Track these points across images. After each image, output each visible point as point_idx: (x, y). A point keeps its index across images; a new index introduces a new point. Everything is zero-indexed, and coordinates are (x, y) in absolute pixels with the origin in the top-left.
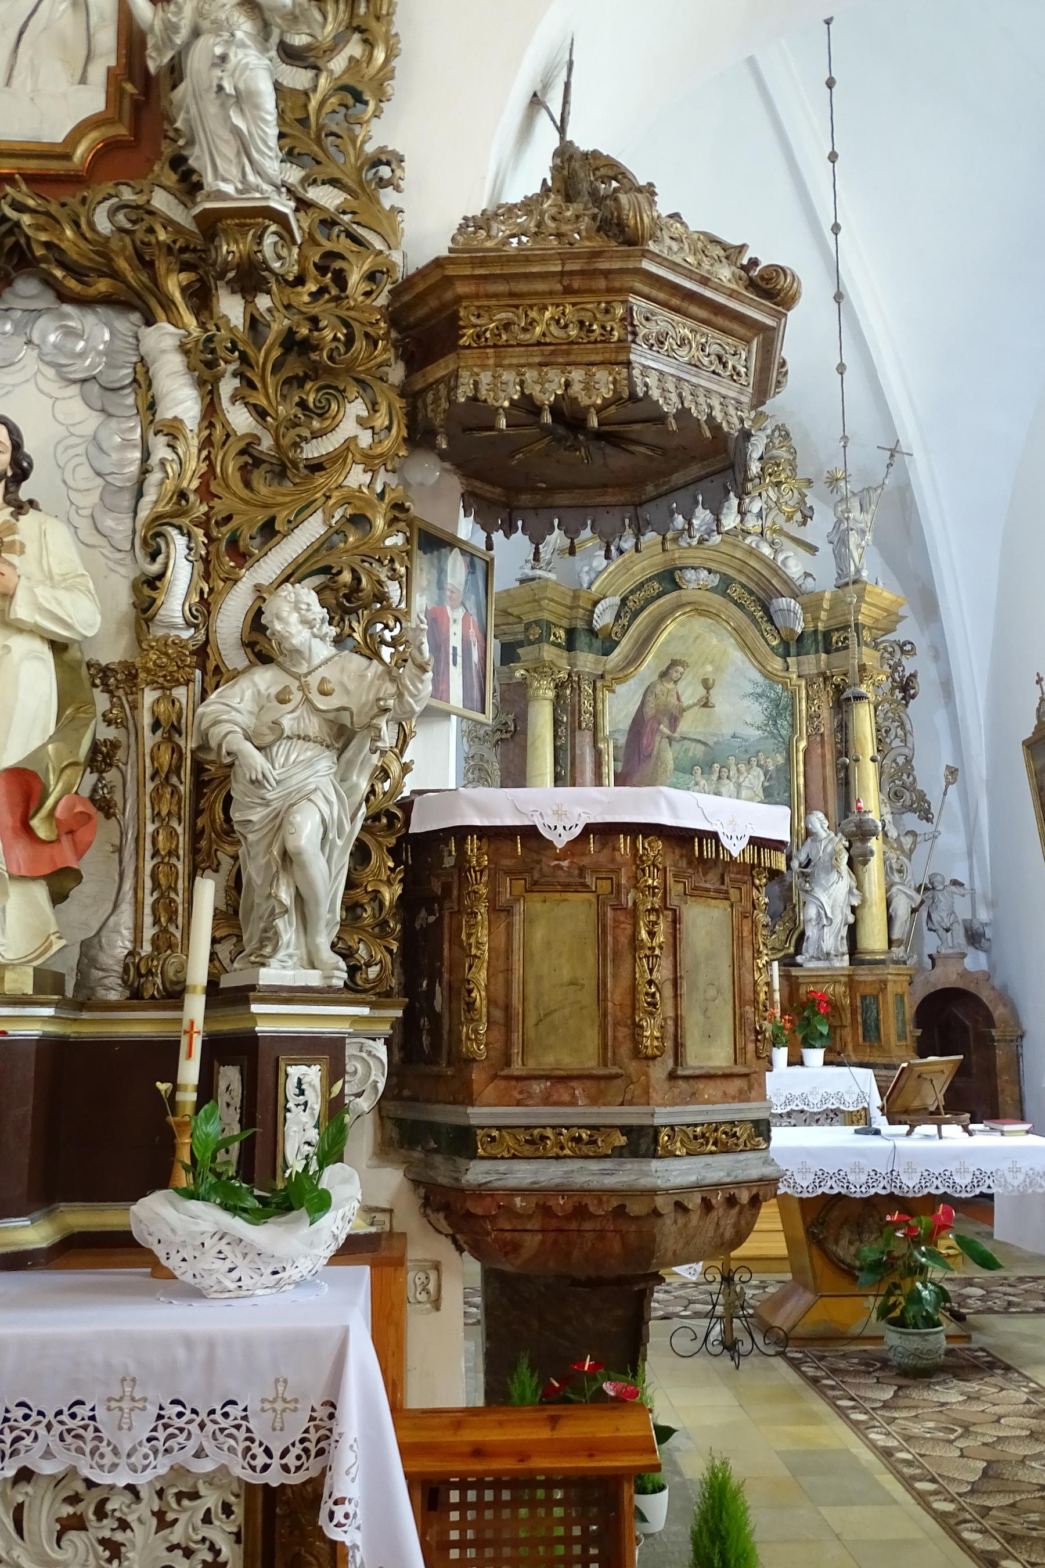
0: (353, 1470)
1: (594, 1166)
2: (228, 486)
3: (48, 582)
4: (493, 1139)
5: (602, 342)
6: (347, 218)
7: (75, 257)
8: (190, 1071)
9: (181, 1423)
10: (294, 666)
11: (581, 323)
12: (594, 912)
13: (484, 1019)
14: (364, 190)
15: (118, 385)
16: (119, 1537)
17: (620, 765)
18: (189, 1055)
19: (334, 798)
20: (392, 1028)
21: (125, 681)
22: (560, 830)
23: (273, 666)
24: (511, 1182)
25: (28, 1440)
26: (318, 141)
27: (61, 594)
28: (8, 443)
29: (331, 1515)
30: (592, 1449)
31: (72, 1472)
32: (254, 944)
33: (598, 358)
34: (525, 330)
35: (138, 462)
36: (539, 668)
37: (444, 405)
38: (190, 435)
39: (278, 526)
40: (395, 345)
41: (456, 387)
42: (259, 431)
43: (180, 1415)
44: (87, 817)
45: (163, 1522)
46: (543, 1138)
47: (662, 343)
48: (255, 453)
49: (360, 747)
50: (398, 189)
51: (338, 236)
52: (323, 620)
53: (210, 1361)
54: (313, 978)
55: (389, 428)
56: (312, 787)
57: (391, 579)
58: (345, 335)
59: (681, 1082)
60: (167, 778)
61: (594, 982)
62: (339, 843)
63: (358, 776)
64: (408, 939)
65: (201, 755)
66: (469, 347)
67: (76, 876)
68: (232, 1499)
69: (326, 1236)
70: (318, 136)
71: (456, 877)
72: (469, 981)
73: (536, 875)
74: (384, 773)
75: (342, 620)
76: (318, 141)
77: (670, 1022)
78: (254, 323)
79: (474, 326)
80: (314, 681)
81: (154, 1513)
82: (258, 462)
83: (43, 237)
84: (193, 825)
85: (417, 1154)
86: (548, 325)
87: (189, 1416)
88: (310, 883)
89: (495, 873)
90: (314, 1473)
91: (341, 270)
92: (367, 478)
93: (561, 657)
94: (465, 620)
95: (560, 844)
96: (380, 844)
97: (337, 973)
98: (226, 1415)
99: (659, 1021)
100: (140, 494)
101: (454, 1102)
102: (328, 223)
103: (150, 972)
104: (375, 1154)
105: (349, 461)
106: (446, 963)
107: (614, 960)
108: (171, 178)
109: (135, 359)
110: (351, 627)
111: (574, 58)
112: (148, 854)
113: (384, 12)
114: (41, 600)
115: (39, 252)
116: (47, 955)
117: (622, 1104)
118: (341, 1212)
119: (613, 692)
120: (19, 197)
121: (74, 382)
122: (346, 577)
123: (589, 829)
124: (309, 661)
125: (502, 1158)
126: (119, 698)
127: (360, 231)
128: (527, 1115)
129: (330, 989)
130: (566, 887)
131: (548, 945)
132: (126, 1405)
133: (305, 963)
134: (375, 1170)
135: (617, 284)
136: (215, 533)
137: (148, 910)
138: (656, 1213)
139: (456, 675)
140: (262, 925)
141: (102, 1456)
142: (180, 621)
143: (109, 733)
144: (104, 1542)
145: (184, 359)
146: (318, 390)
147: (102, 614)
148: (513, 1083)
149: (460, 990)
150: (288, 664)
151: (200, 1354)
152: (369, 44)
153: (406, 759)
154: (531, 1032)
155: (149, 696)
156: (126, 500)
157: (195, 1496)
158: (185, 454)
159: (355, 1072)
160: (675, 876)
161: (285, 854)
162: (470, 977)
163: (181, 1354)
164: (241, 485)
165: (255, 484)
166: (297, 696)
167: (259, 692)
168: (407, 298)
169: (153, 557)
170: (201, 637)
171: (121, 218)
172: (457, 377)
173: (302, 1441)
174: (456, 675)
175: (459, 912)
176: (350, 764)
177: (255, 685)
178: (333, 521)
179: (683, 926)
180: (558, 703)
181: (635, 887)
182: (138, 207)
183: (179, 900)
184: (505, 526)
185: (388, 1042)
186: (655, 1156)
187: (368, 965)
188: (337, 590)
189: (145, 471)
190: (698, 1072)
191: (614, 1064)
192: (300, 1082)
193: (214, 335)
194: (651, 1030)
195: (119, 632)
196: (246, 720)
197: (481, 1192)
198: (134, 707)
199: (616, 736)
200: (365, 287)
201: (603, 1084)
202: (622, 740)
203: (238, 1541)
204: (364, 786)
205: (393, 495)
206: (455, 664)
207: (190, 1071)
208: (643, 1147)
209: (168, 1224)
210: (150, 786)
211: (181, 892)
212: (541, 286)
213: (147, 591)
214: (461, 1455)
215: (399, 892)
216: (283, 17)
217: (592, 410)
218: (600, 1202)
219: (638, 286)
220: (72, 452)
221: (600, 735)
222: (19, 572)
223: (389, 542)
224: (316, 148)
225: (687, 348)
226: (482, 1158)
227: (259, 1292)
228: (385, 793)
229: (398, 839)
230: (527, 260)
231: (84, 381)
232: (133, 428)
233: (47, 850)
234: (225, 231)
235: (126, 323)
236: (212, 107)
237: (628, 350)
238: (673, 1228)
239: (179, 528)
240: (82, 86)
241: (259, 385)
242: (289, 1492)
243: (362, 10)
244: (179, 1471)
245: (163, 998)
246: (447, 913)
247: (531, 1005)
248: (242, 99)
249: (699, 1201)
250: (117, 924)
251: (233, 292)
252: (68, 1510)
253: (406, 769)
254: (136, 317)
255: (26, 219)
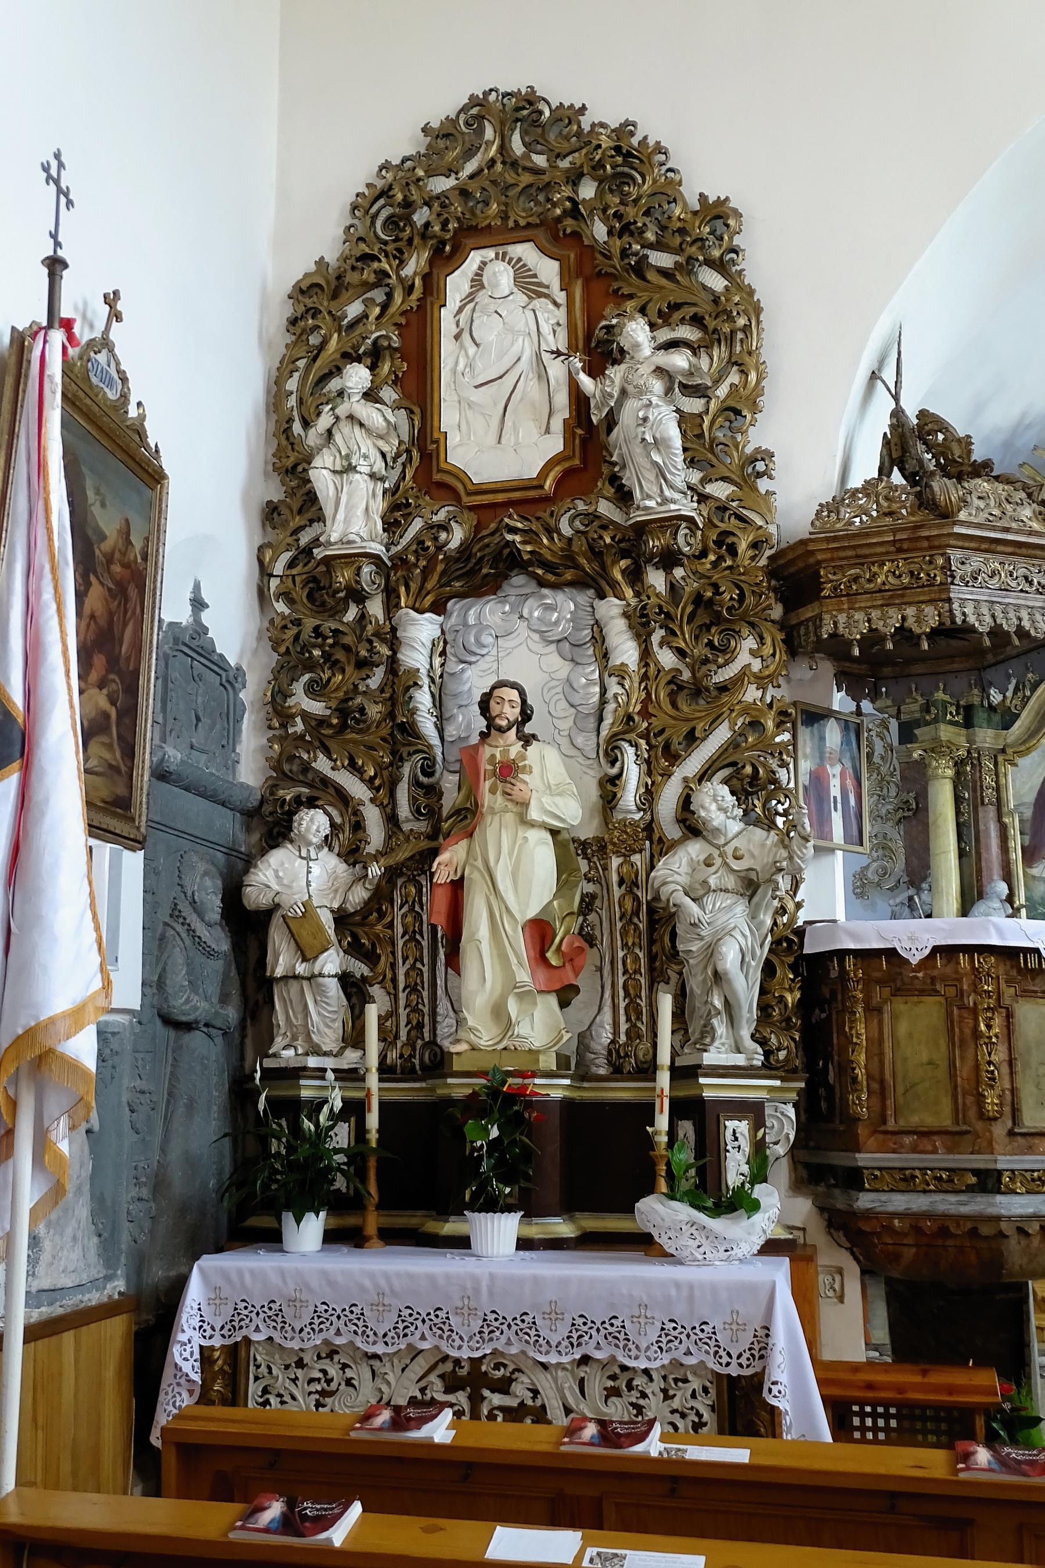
0: (782, 1366)
1: (952, 1198)
2: (661, 708)
3: (548, 791)
4: (876, 1177)
5: (928, 586)
6: (734, 504)
7: (549, 558)
8: (662, 1122)
9: (675, 1333)
10: (715, 838)
11: (912, 573)
12: (943, 1010)
13: (865, 1090)
14: (746, 482)
15: (581, 642)
16: (641, 1402)
17: (1027, 838)
18: (662, 1111)
19: (748, 933)
20: (798, 1095)
21: (598, 851)
22: (914, 951)
23: (700, 838)
24: (890, 1208)
25: (586, 1338)
26: (712, 451)
27: (558, 800)
28: (519, 701)
29: (770, 1391)
30: (951, 1390)
31: (613, 1359)
32: (697, 1035)
33: (927, 598)
34: (869, 581)
35: (598, 695)
36: (936, 748)
37: (813, 638)
38: (633, 674)
39: (698, 734)
40: (775, 590)
41: (821, 627)
42: (681, 666)
43: (675, 1329)
44: (581, 950)
45: (667, 1397)
46: (914, 1177)
47: (976, 579)
48: (679, 682)
49: (764, 893)
50: (771, 477)
51: (729, 518)
52: (733, 806)
53: (691, 1299)
54: (740, 1060)
55: (774, 655)
56: (732, 925)
57: (780, 766)
58: (738, 595)
59: (1019, 1138)
60: (631, 919)
61: (947, 1062)
62: (753, 963)
63: (764, 915)
64: (807, 1030)
65: (654, 904)
66: (829, 597)
67: (575, 989)
68: (708, 1384)
69: (759, 1230)
70: (711, 446)
71: (839, 986)
72: (852, 1062)
73: (899, 984)
74: (782, 911)
75: (747, 798)
76: (712, 451)
77: (1007, 1092)
78: (673, 588)
79: (832, 581)
80: (729, 850)
81: (662, 1390)
82: (681, 688)
83: (529, 548)
84: (650, 951)
85: (821, 1189)
86: (887, 577)
87: (680, 1329)
88: (734, 992)
89: (868, 983)
90: (758, 1369)
91: (733, 543)
92: (759, 693)
93: (959, 735)
94: (842, 774)
95: (914, 961)
96: (783, 961)
97: (756, 1056)
98: (702, 1331)
99: (998, 1091)
100: (601, 720)
101: (847, 1150)
102: (722, 509)
103: (627, 1055)
104: (790, 1188)
105: (746, 682)
106: (836, 1048)
107: (960, 1046)
108: (609, 491)
109: (592, 622)
110: (753, 804)
111: (902, 349)
112: (620, 972)
113: (754, 348)
114: (546, 805)
115: (526, 557)
116: (560, 1044)
117: (972, 1153)
118: (767, 1215)
119: (1016, 765)
120: (512, 523)
121: (552, 642)
122: (749, 769)
123: (936, 949)
124: (725, 835)
125: (884, 1191)
126: (595, 863)
127: (745, 512)
128: (901, 1160)
129: (752, 1067)
130: (922, 993)
131: (910, 1035)
132: (642, 1320)
133: (733, 1049)
134: (792, 1199)
135: (936, 543)
136: (653, 742)
137: (622, 1012)
138: (1002, 1235)
139: (837, 819)
140: (702, 1022)
141: (630, 1350)
142: (634, 808)
143: (590, 888)
144: (634, 1405)
145: (627, 621)
146: (720, 633)
147: (582, 808)
148: (889, 1136)
149: (846, 1068)
150: (710, 838)
151: (685, 1292)
152: (744, 373)
153: (798, 899)
154: (901, 1100)
155: (615, 862)
156: (592, 723)
157: (686, 1381)
158: (630, 688)
159: (773, 1127)
160: (1006, 982)
161: (716, 973)
162: (853, 1058)
163: (673, 1292)
164: (670, 707)
165: (680, 705)
166: (718, 861)
167: (692, 859)
168: (781, 562)
169: (613, 763)
170: (648, 817)
171: (577, 523)
172: (821, 620)
173: (750, 1349)
174: (837, 819)
175: (843, 1011)
176: (758, 906)
177: (689, 854)
178: (737, 728)
179: (1016, 1020)
180: (958, 782)
181: (975, 992)
182: (588, 514)
183: (643, 1004)
184: (872, 694)
185: (796, 1106)
186: (1000, 1192)
187: (779, 1049)
188: (742, 780)
189: (603, 702)
190: (1033, 1130)
191: (965, 1123)
192: (734, 1131)
193: (646, 604)
194: (991, 1099)
195: (592, 816)
196: (683, 879)
197: (868, 1215)
198: (605, 868)
199: (1022, 809)
200: (750, 553)
201: (956, 1138)
202: (1028, 813)
203: (713, 1411)
204: (769, 922)
205: (780, 704)
206: (836, 810)
207: (662, 1122)
208: (990, 1186)
209: (659, 1215)
210: (619, 925)
211: (644, 999)
212: (879, 550)
213: (609, 787)
214: (859, 1388)
215: (799, 996)
216: (683, 375)
217: (924, 637)
218: (958, 1225)
219: (952, 542)
220: (553, 691)
221: (1005, 810)
222: (531, 786)
223: (778, 739)
224: (710, 456)
225: (997, 578)
226: (868, 1190)
227: (717, 1263)
228: (784, 925)
229: (796, 958)
230: (867, 535)
231: (559, 641)
232: (594, 671)
233: (557, 972)
234: (651, 532)
235: (585, 597)
236: (638, 450)
237: (948, 591)
238: (1017, 1247)
239: (630, 742)
240: (547, 436)
241: (679, 633)
242: (743, 1382)
243: (738, 349)
244: (676, 1364)
245: (636, 1073)
246: (834, 1012)
247: (899, 1079)
248: (658, 443)
249: (1038, 1228)
250: (602, 1022)
251: (657, 569)
252: (610, 1383)
253: (799, 906)
254: (591, 592)
255: (518, 538)
